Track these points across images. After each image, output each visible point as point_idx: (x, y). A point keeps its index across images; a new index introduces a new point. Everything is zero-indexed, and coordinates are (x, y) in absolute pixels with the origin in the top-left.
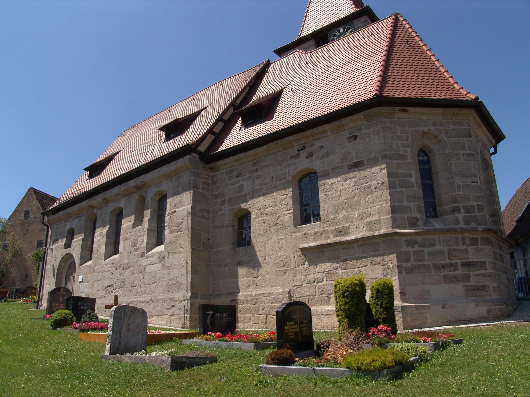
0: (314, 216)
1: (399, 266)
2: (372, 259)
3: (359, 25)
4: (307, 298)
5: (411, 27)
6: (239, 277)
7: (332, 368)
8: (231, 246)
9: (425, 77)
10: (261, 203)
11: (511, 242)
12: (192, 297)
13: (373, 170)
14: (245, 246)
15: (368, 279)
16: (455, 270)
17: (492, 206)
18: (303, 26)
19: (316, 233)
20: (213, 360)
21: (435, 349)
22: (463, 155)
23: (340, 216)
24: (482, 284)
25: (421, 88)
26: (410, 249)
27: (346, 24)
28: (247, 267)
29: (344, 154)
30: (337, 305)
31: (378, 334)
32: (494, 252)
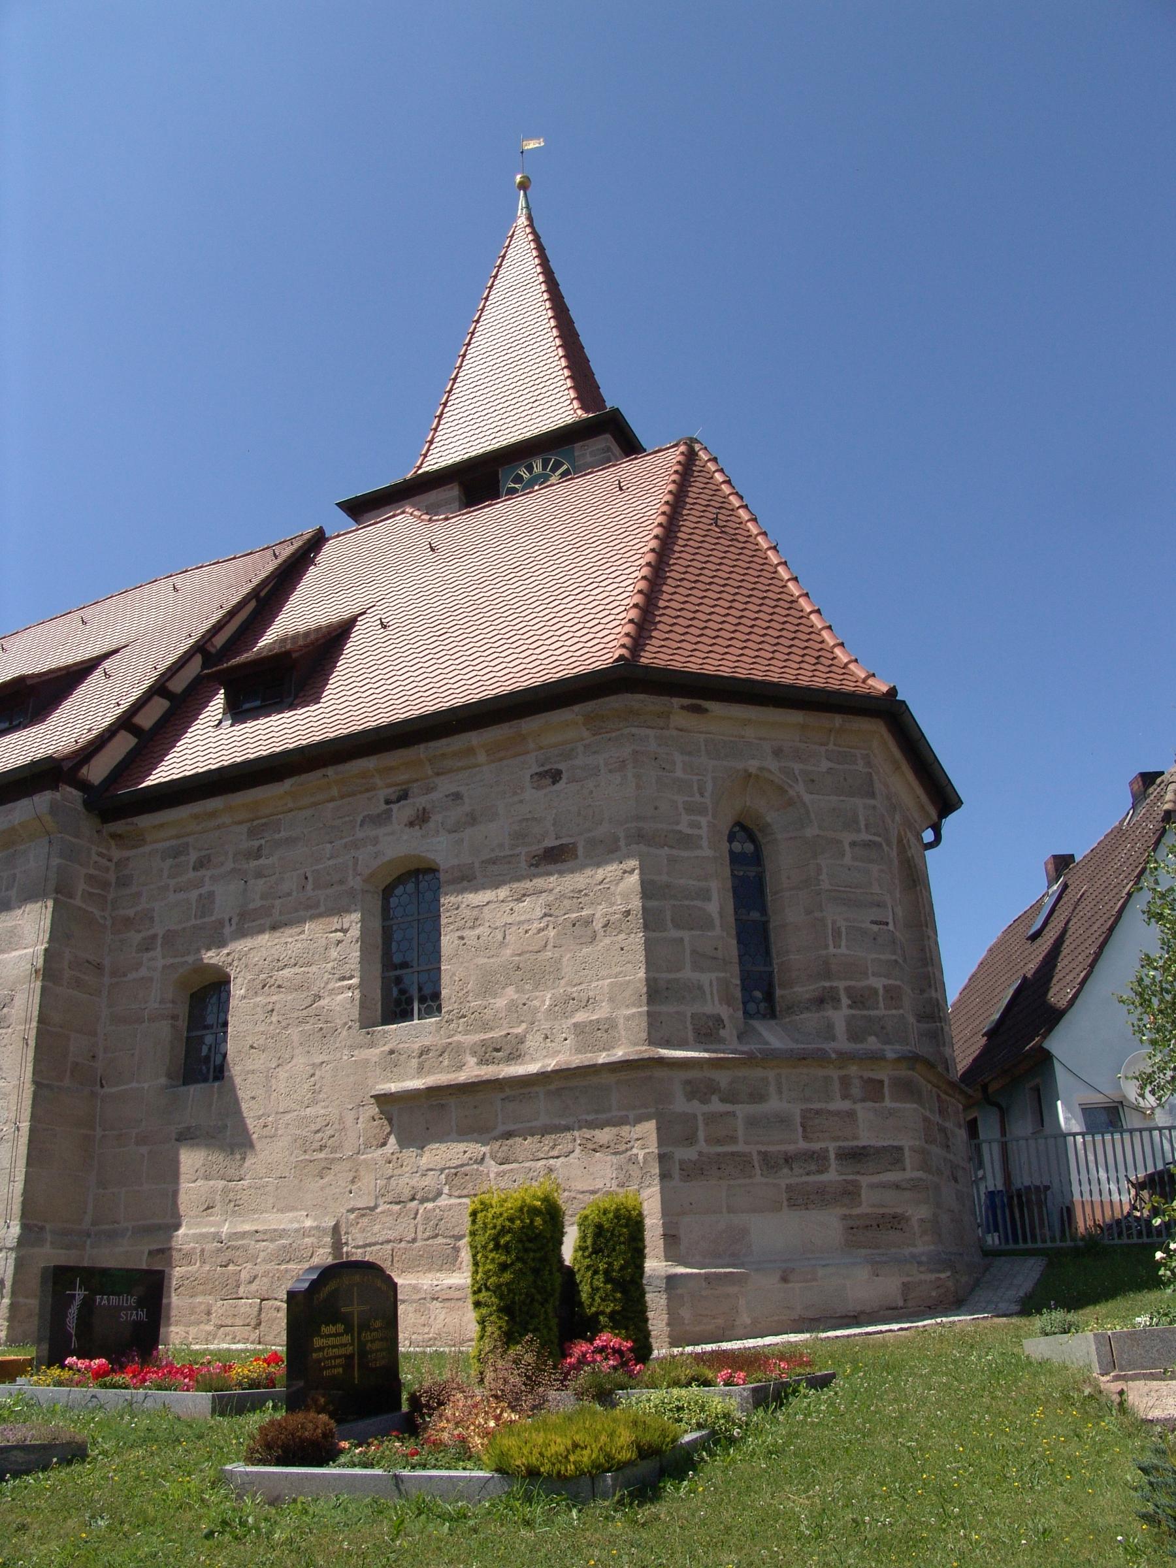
0: (422, 1000)
1: (662, 1158)
2: (587, 1133)
3: (589, 459)
4: (389, 1246)
5: (728, 482)
6: (183, 1178)
7: (453, 1473)
8: (163, 1080)
9: (758, 622)
10: (264, 953)
11: (970, 1091)
12: (22, 1241)
13: (600, 873)
14: (205, 1080)
15: (573, 1194)
16: (820, 1172)
17: (922, 991)
18: (431, 442)
20: (74, 1453)
21: (757, 1405)
22: (853, 844)
23: (500, 1003)
24: (891, 1211)
25: (746, 651)
26: (696, 1107)
27: (552, 452)
28: (208, 1146)
29: (521, 821)
30: (476, 1272)
31: (594, 1361)
32: (925, 1119)
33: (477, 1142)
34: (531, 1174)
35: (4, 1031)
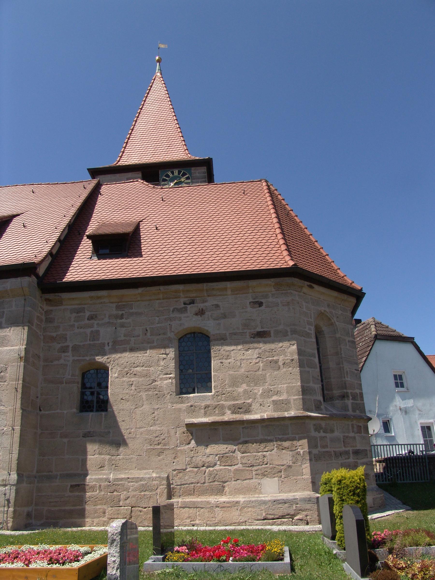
1: (310, 453)
2: (279, 443)
4: (193, 485)
6: (89, 453)
8: (75, 410)
10: (127, 360)
13: (281, 344)
15: (274, 466)
19: (207, 407)
23: (241, 390)
33: (232, 444)
34: (256, 458)
35: (2, 383)
